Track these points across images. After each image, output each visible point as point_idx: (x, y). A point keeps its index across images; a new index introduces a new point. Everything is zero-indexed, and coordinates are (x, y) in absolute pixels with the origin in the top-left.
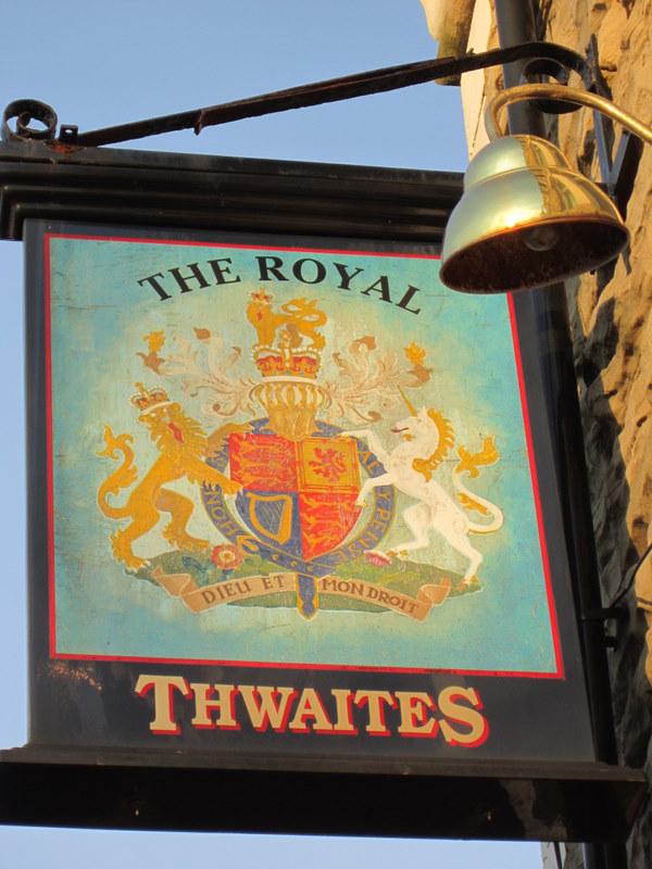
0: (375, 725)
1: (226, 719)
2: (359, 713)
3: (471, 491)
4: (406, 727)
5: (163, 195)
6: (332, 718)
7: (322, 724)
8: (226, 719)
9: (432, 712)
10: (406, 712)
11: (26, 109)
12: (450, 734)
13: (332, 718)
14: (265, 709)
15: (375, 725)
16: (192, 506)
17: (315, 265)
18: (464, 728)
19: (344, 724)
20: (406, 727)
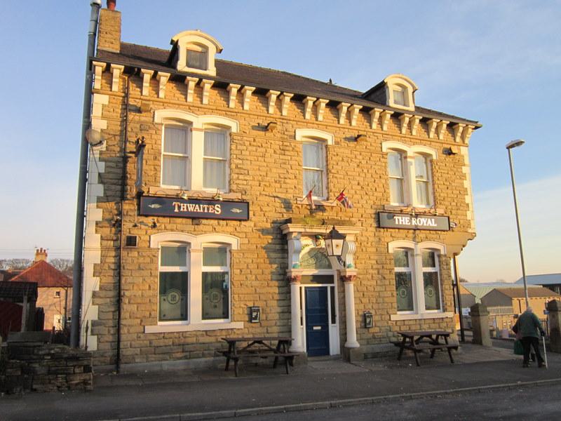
0: (206, 211)
1: (185, 210)
2: (204, 209)
3: (171, 185)
4: (210, 211)
5: (309, 404)
6: (398, 219)
7: (199, 211)
8: (185, 210)
9: (214, 209)
10: (210, 209)
11: (41, 252)
12: (216, 213)
13: (398, 219)
14: (213, 378)
15: (206, 211)
16: (43, 261)
17: (215, 47)
18: (218, 211)
19: (202, 211)
20: (210, 211)
